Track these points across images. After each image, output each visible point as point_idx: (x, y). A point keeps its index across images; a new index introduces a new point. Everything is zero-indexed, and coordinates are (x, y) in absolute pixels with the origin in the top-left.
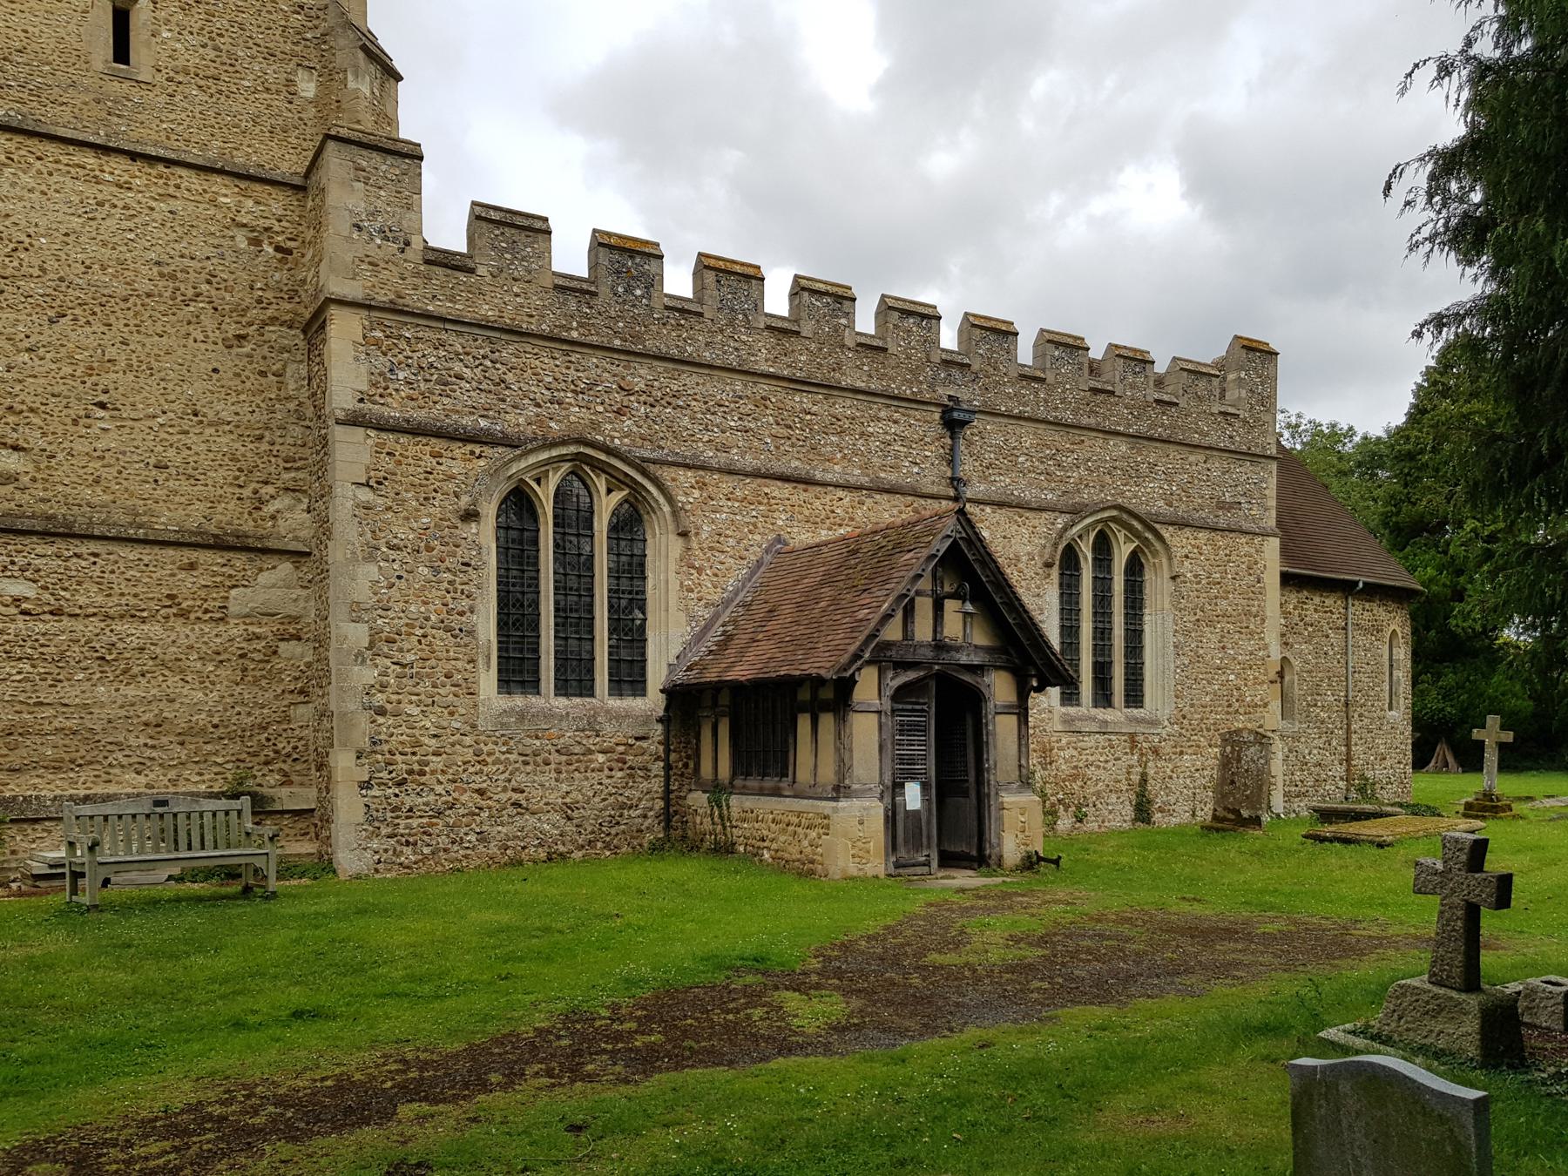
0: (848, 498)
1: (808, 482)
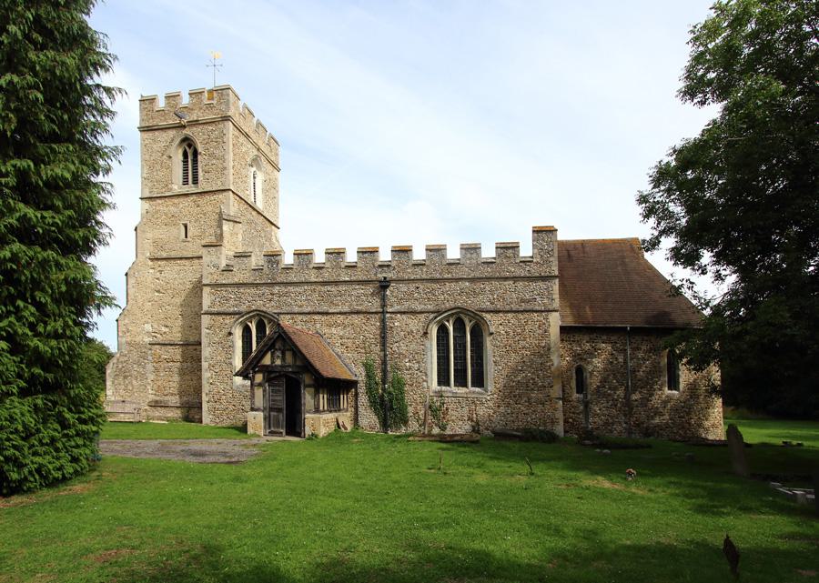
0: (342, 317)
1: (327, 313)
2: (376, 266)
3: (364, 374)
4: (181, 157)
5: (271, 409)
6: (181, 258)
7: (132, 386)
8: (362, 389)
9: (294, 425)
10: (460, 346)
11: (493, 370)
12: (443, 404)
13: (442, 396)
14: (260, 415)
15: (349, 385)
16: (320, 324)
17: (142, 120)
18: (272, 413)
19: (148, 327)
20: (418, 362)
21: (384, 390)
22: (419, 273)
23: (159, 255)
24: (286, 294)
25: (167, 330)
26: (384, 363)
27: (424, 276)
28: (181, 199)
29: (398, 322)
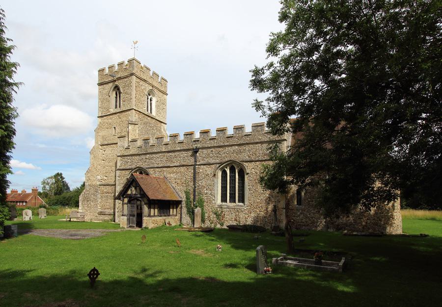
1: (169, 167)
2: (192, 141)
3: (185, 197)
4: (115, 95)
5: (131, 215)
6: (112, 144)
7: (91, 205)
8: (184, 204)
9: (139, 224)
10: (233, 181)
11: (248, 193)
12: (222, 212)
13: (222, 208)
14: (125, 218)
15: (176, 204)
16: (166, 173)
17: (99, 80)
18: (131, 217)
19: (99, 177)
20: (211, 190)
21: (194, 205)
22: (214, 143)
23: (103, 144)
24: (152, 159)
25: (106, 178)
26: (194, 191)
27: (215, 145)
28: (113, 116)
29: (201, 170)
